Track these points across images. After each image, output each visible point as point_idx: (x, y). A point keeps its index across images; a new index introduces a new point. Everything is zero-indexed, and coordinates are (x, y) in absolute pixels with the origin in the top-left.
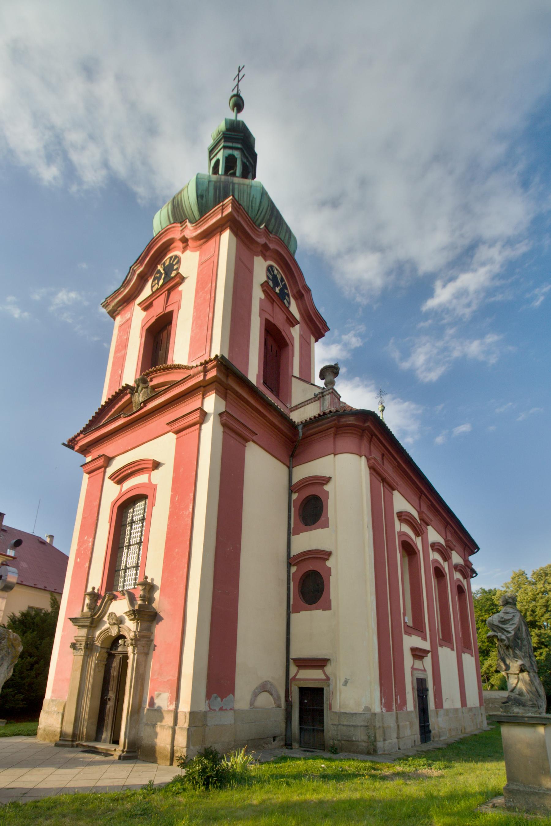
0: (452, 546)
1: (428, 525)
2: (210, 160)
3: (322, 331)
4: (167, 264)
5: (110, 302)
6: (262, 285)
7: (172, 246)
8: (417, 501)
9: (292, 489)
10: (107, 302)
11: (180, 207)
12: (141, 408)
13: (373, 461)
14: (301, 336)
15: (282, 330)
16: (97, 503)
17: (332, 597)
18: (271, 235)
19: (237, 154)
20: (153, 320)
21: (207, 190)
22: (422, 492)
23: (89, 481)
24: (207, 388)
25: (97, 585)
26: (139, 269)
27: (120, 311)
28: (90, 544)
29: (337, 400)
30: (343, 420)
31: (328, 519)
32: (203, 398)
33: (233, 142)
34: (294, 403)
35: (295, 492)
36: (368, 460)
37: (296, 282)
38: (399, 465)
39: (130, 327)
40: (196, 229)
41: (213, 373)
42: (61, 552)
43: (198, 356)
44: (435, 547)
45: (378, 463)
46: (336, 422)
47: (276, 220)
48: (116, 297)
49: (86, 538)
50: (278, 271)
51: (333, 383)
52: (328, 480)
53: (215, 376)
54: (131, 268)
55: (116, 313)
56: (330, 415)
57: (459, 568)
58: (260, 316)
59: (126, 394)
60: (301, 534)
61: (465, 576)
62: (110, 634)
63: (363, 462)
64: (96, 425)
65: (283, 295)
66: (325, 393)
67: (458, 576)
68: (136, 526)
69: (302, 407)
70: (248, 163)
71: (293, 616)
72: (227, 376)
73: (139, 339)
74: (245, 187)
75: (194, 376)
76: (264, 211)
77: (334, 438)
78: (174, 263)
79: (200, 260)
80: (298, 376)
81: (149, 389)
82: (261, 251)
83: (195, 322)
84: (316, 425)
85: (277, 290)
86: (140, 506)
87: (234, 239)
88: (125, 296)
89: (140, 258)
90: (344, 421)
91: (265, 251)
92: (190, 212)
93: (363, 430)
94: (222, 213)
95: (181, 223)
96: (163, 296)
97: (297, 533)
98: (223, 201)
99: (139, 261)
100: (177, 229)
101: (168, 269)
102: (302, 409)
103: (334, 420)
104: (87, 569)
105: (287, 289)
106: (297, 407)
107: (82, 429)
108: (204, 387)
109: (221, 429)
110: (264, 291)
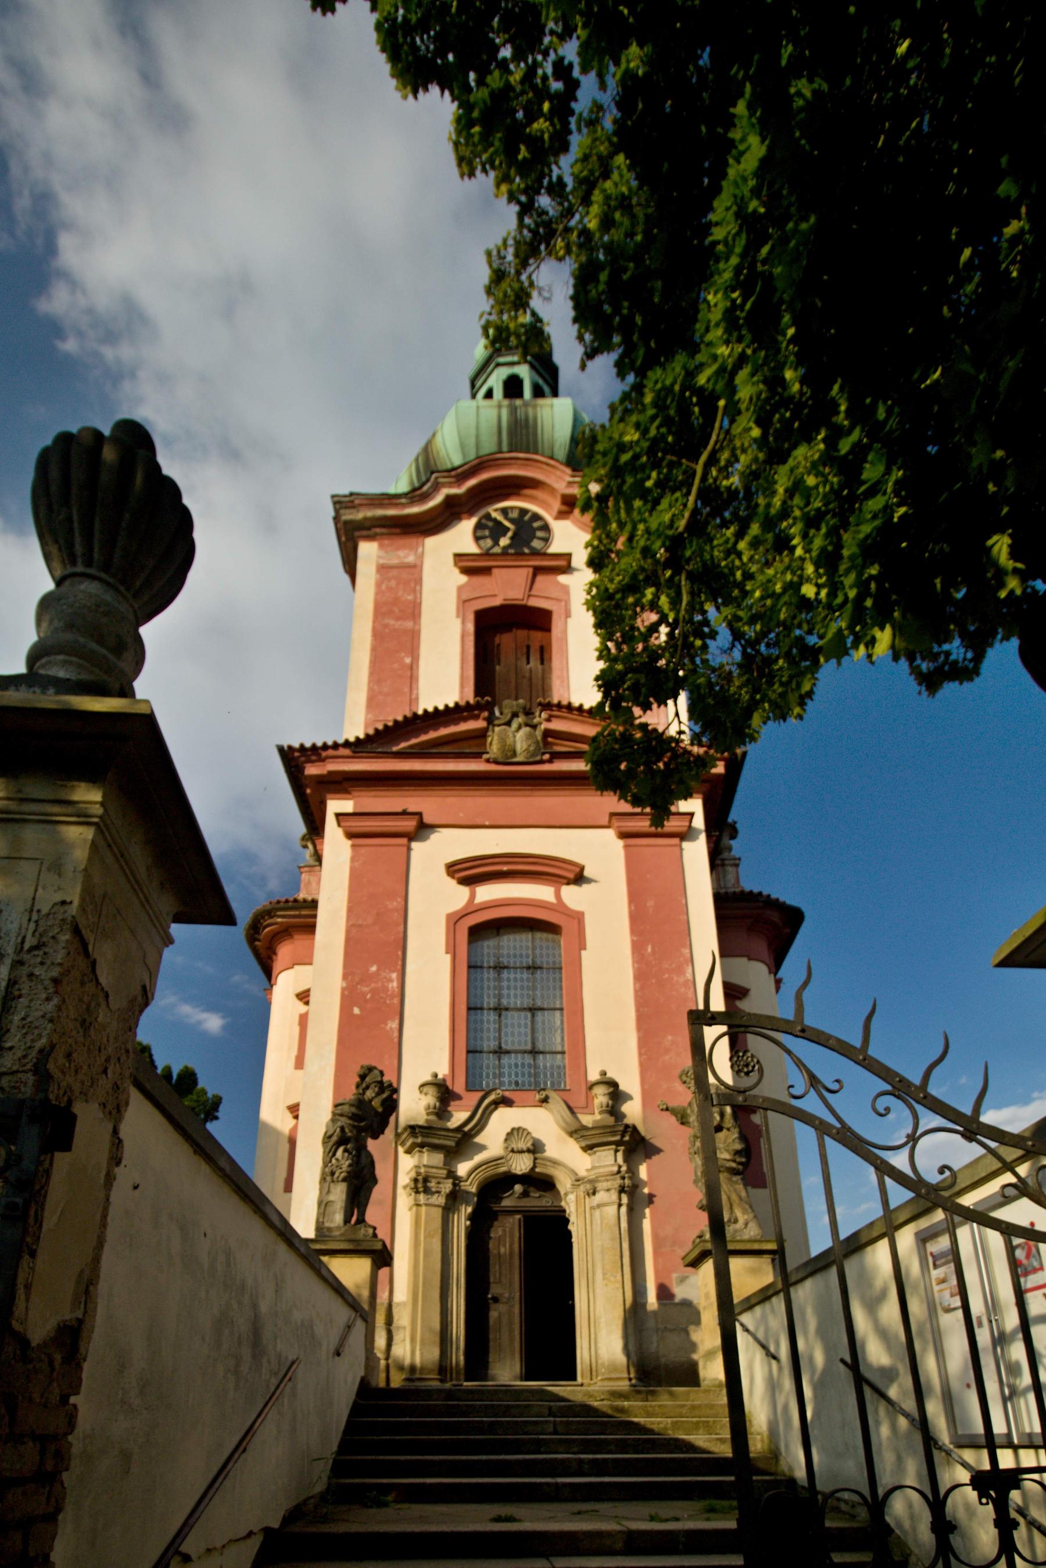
5: (361, 505)
10: (352, 502)
12: (542, 762)
20: (497, 602)
48: (381, 506)
55: (365, 533)
59: (476, 717)
66: (727, 862)
73: (458, 622)
89: (459, 470)
104: (396, 1034)
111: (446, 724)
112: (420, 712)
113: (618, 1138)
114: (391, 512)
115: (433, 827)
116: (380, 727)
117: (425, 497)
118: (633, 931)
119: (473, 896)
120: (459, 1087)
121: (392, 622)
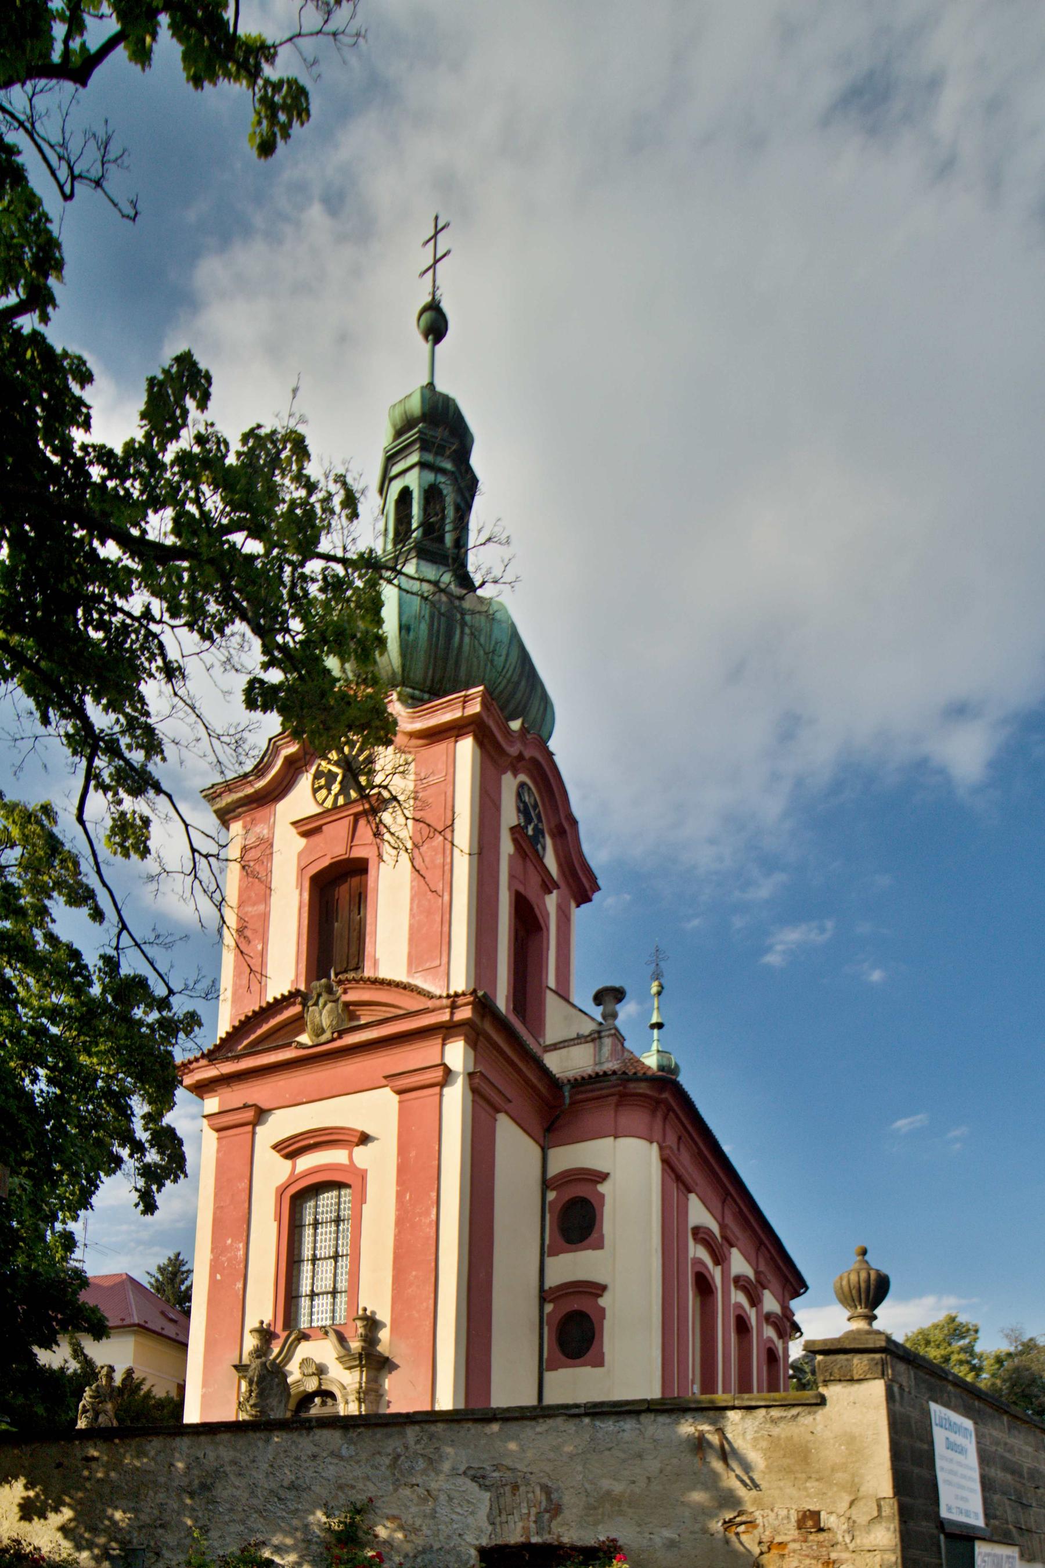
0: (765, 1281)
1: (732, 1246)
2: (386, 480)
3: (590, 893)
6: (513, 830)
8: (719, 1205)
12: (333, 1040)
15: (535, 906)
17: (606, 1349)
20: (325, 862)
22: (728, 1193)
23: (219, 1143)
24: (452, 1030)
25: (268, 1317)
26: (288, 747)
28: (241, 1253)
29: (620, 1046)
30: (632, 1085)
32: (444, 1045)
36: (661, 1148)
37: (557, 808)
38: (700, 1152)
40: (413, 718)
41: (465, 1013)
43: (427, 966)
44: (740, 1282)
46: (621, 1088)
49: (229, 1241)
50: (533, 796)
51: (614, 1015)
52: (604, 1177)
53: (468, 1019)
54: (270, 740)
55: (232, 815)
56: (615, 1077)
57: (772, 1319)
58: (510, 889)
59: (294, 1004)
60: (561, 1256)
61: (781, 1335)
62: (302, 1388)
63: (653, 1152)
66: (603, 1034)
67: (770, 1332)
71: (548, 1376)
72: (483, 1017)
75: (433, 1011)
76: (512, 667)
77: (616, 1112)
81: (340, 1006)
83: (416, 902)
86: (328, 1199)
87: (478, 751)
91: (516, 765)
93: (658, 1102)
94: (464, 708)
96: (346, 821)
98: (467, 689)
102: (564, 1051)
104: (241, 1292)
106: (555, 1047)
110: (515, 841)
111: (274, 1016)
113: (357, 1363)
115: (269, 1111)
116: (243, 1018)
117: (269, 766)
118: (398, 1183)
120: (279, 1329)
121: (250, 909)
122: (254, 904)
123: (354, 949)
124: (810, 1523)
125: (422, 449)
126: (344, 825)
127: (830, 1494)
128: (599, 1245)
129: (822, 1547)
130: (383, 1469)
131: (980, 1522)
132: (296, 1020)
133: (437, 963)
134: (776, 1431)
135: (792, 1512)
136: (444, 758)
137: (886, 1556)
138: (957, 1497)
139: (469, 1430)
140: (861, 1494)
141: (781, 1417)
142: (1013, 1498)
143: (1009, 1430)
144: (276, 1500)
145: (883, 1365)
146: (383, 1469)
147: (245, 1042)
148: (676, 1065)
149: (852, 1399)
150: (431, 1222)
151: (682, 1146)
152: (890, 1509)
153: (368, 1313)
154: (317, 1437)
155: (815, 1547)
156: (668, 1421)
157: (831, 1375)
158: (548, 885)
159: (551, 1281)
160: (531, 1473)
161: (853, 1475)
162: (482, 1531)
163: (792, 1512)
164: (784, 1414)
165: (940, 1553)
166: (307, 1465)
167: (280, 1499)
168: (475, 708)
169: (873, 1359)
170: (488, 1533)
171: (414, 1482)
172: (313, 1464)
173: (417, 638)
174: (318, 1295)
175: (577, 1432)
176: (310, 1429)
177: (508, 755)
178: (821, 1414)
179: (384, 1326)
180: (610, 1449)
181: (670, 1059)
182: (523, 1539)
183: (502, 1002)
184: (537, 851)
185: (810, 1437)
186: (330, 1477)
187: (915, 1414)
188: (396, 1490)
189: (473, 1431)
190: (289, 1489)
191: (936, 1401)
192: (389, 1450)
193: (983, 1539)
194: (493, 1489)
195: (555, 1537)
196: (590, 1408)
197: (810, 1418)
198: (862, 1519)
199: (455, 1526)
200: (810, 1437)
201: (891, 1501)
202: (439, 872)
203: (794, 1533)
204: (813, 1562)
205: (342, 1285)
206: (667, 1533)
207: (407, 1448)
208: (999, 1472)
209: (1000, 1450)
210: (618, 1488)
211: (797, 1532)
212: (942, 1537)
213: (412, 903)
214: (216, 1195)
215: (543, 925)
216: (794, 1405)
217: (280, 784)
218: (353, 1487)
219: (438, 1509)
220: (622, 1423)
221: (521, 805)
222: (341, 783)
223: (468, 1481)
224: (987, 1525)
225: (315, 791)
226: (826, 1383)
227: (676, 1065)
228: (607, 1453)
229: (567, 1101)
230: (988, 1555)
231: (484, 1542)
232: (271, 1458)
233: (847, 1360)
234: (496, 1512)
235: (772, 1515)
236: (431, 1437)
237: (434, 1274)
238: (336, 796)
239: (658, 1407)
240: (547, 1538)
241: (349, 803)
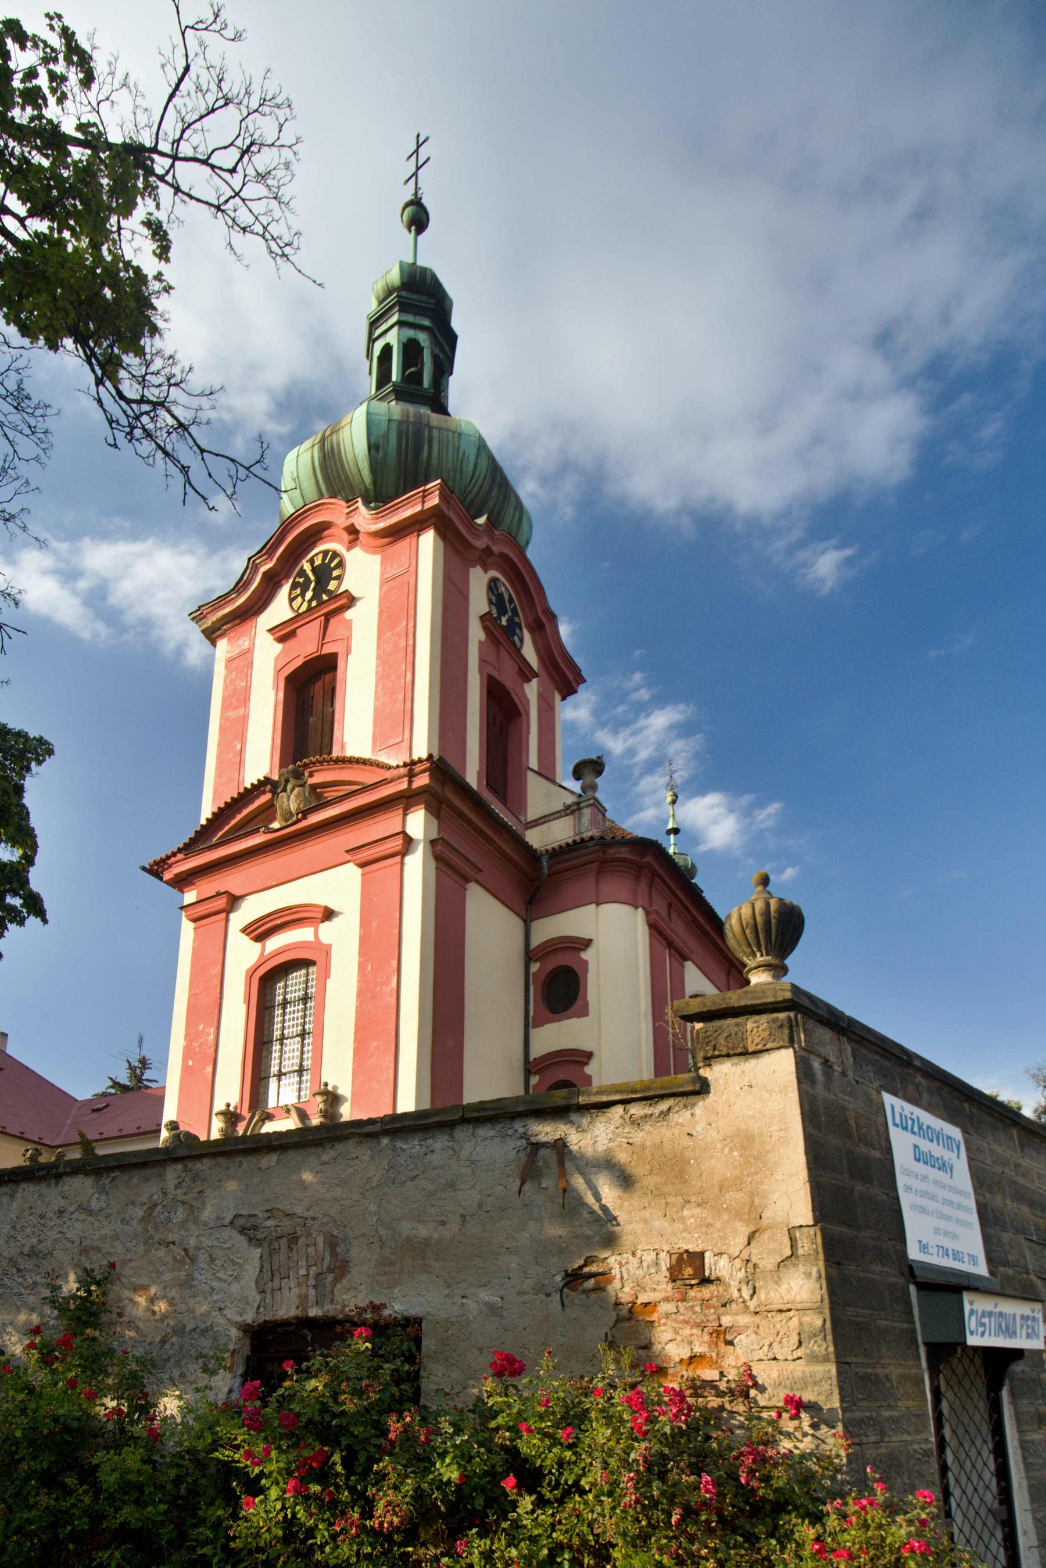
2: (372, 340)
3: (574, 684)
4: (318, 562)
6: (483, 618)
7: (327, 533)
8: (724, 978)
9: (530, 955)
11: (337, 458)
12: (298, 821)
13: (654, 916)
14: (541, 697)
15: (511, 691)
16: (217, 970)
18: (496, 532)
19: (423, 338)
20: (299, 662)
21: (386, 436)
24: (412, 800)
25: (234, 1100)
27: (226, 631)
28: (212, 1037)
29: (600, 816)
31: (586, 1003)
32: (405, 815)
33: (415, 314)
34: (532, 814)
35: (535, 961)
36: (647, 913)
39: (250, 665)
40: (376, 519)
41: (422, 780)
42: (21, 1064)
43: (391, 743)
45: (663, 920)
46: (600, 854)
47: (500, 487)
48: (221, 607)
49: (201, 1027)
50: (506, 587)
51: (594, 787)
52: (587, 943)
54: (249, 559)
55: (219, 633)
56: (592, 843)
58: (480, 671)
59: (264, 792)
60: (547, 1026)
64: (206, 841)
65: (513, 627)
66: (582, 805)
68: (292, 1009)
69: (545, 822)
70: (441, 356)
72: (444, 784)
73: (273, 693)
74: (450, 434)
75: (392, 781)
77: (597, 878)
78: (332, 565)
79: (382, 573)
80: (536, 769)
81: (307, 789)
82: (480, 557)
83: (381, 684)
84: (568, 856)
85: (504, 621)
86: (297, 977)
87: (441, 544)
88: (239, 607)
90: (614, 852)
91: (486, 557)
92: (354, 470)
93: (641, 867)
94: (423, 502)
95: (347, 501)
96: (317, 623)
97: (539, 1024)
99: (267, 550)
100: (339, 508)
101: (324, 574)
103: (598, 851)
104: (210, 1077)
105: (518, 616)
106: (536, 823)
107: (181, 846)
108: (407, 798)
109: (433, 864)
110: (485, 628)
111: (246, 806)
112: (249, 786)
114: (228, 609)
115: (242, 897)
119: (263, 949)
120: (245, 1112)
121: (231, 714)
122: (235, 709)
123: (326, 740)
124: (688, 1271)
125: (400, 311)
126: (316, 626)
127: (718, 1225)
128: (584, 1012)
129: (708, 1307)
130: (135, 1223)
131: (981, 1269)
132: (268, 808)
133: (401, 739)
134: (638, 1136)
135: (663, 1255)
136: (408, 552)
137: (807, 1319)
138: (954, 1236)
139: (241, 1164)
140: (764, 1222)
141: (646, 1116)
142: (1034, 1238)
143: (1022, 1147)
144: (14, 1271)
145: (791, 1027)
146: (135, 1223)
147: (220, 834)
148: (692, 864)
149: (746, 1081)
150: (391, 990)
151: (674, 916)
152: (810, 1243)
153: (330, 1088)
154: (66, 1188)
155: (697, 1309)
156: (491, 1133)
157: (715, 1048)
158: (526, 673)
159: (536, 1052)
160: (314, 1219)
161: (752, 1195)
162: (248, 1303)
163: (663, 1255)
164: (648, 1111)
165: (910, 1313)
166: (52, 1223)
167: (19, 1270)
168: (434, 500)
169: (774, 1021)
170: (256, 1305)
171: (171, 1239)
172: (59, 1222)
173: (385, 455)
174: (285, 1074)
175: (372, 1158)
176: (59, 1176)
177: (475, 548)
178: (701, 1107)
179: (346, 1100)
180: (413, 1179)
181: (686, 860)
182: (299, 1313)
183: (472, 775)
184: (514, 643)
185: (687, 1141)
186: (75, 1239)
187: (854, 1106)
188: (148, 1251)
189: (245, 1166)
190: (28, 1256)
191: (895, 1093)
192: (144, 1198)
193: (976, 1290)
194: (266, 1244)
195: (339, 1307)
196: (388, 1123)
197: (687, 1114)
198: (768, 1262)
199: (215, 1297)
200: (687, 1141)
201: (812, 1231)
202: (402, 654)
203: (666, 1288)
204: (695, 1331)
205: (307, 1063)
206: (485, 1295)
207: (165, 1194)
208: (1008, 1202)
209: (1009, 1173)
210: (423, 1232)
211: (670, 1285)
212: (912, 1289)
213: (376, 687)
214: (191, 983)
215: (522, 710)
216: (663, 1097)
217: (260, 599)
218: (98, 1249)
219: (196, 1275)
220: (430, 1141)
221: (494, 598)
222: (314, 590)
223: (235, 1234)
224: (991, 1272)
225: (291, 600)
226: (708, 1060)
227: (692, 864)
228: (410, 1184)
229: (546, 871)
230: (990, 1314)
231: (249, 1317)
232: (14, 1216)
233: (737, 1025)
234: (267, 1276)
235: (634, 1261)
236: (195, 1177)
237: (394, 1042)
238: (310, 601)
239: (476, 1115)
240: (330, 1309)
241: (321, 603)
